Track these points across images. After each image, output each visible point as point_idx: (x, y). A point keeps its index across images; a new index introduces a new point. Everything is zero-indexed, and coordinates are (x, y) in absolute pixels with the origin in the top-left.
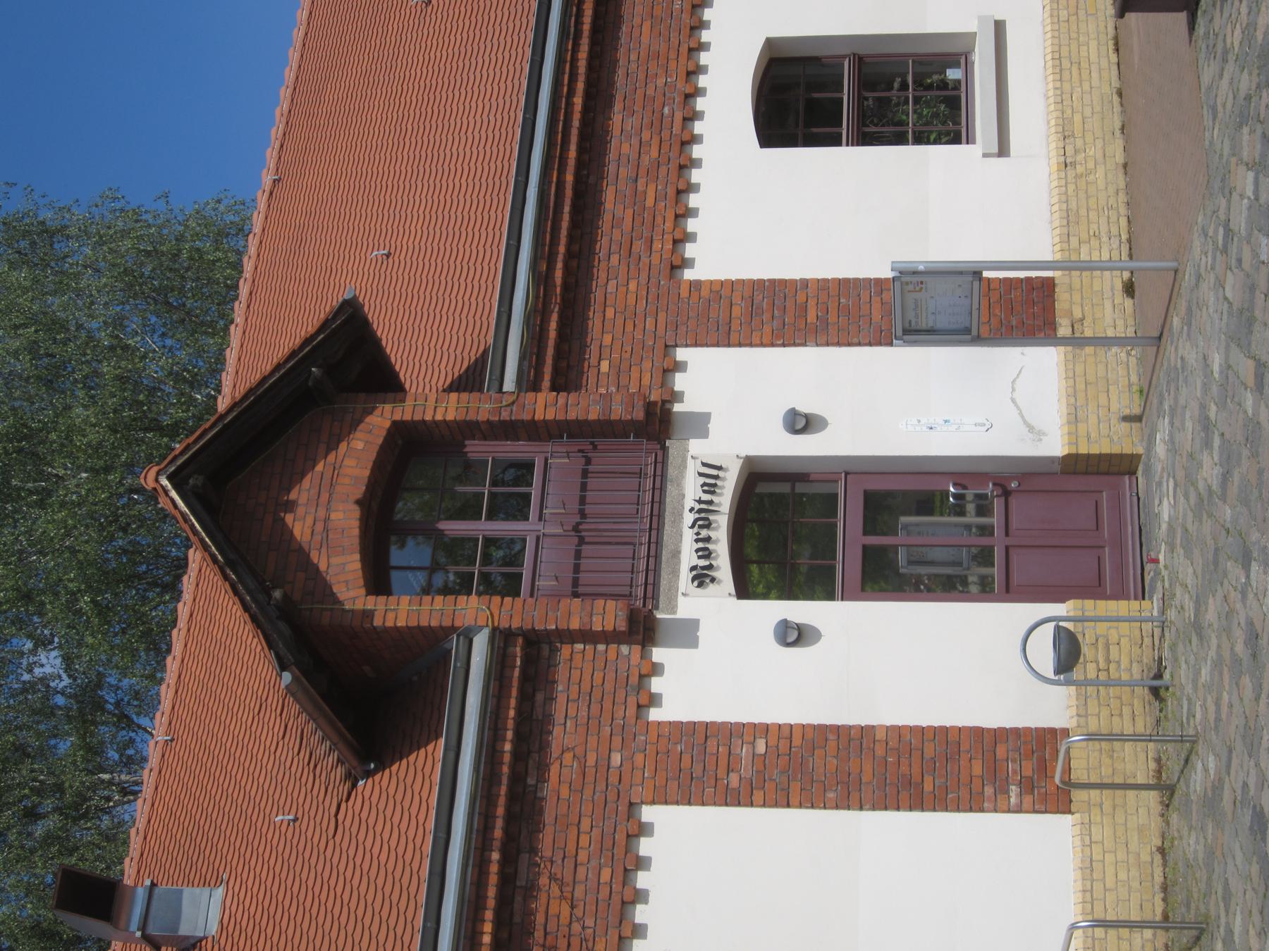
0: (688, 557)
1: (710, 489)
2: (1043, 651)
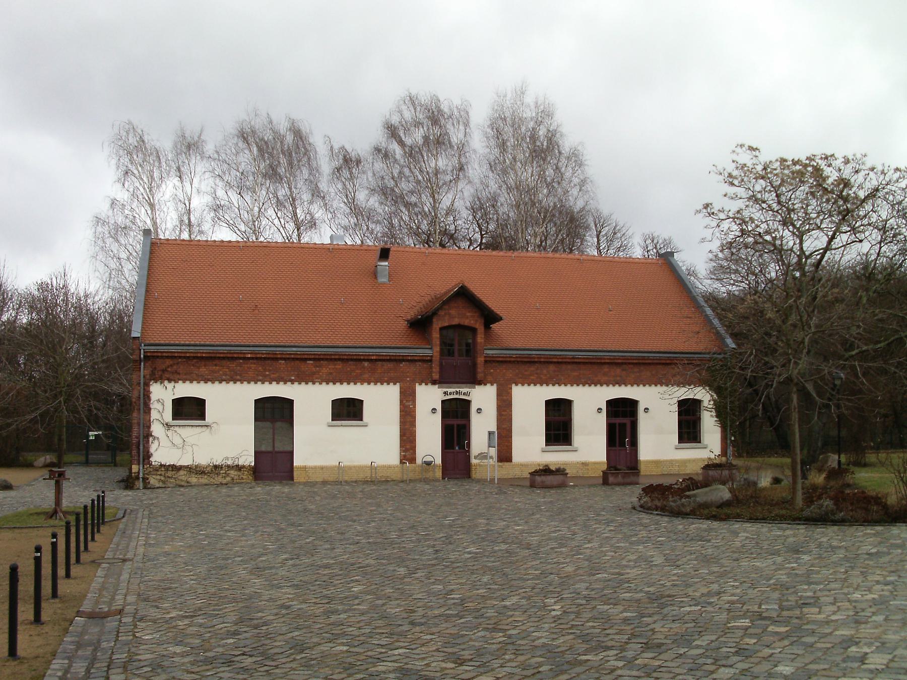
0: (449, 390)
1: (464, 394)
2: (429, 459)
